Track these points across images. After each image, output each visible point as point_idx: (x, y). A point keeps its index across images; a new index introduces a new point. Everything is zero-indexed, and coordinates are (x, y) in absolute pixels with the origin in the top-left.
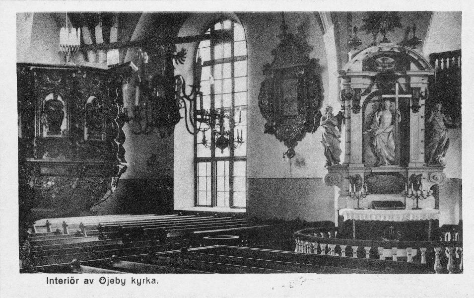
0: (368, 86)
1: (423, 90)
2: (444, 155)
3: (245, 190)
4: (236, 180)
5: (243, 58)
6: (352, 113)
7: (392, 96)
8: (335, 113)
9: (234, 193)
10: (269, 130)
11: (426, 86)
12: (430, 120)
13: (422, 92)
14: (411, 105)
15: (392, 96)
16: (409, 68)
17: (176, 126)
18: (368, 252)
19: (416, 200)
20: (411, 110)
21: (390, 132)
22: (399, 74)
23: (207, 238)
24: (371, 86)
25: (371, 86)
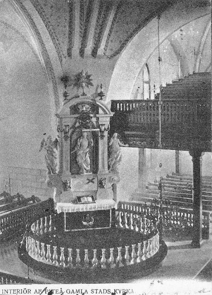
12: (110, 144)
14: (99, 135)
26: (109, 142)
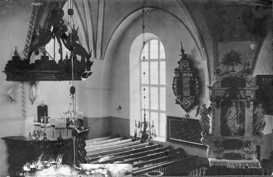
0: (224, 94)
1: (252, 96)
2: (263, 130)
3: (165, 128)
4: (161, 70)
5: (163, 60)
6: (215, 108)
7: (236, 100)
8: (207, 107)
9: (151, 44)
10: (177, 103)
11: (254, 94)
12: (255, 112)
13: (252, 98)
14: (246, 105)
15: (236, 100)
16: (245, 86)
17: (91, 67)
18: (78, 131)
19: (249, 155)
20: (246, 107)
21: (235, 119)
22: (240, 89)
23: (157, 149)
24: (226, 94)
25: (226, 94)
26: (254, 110)
